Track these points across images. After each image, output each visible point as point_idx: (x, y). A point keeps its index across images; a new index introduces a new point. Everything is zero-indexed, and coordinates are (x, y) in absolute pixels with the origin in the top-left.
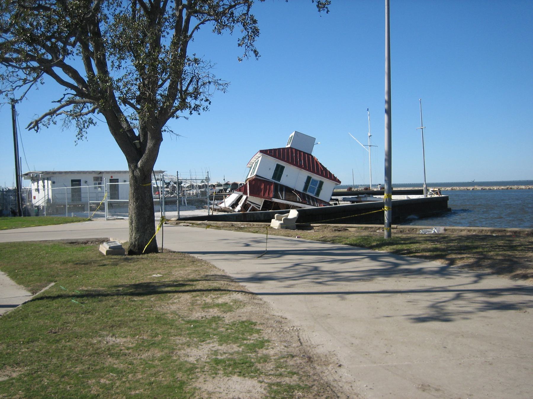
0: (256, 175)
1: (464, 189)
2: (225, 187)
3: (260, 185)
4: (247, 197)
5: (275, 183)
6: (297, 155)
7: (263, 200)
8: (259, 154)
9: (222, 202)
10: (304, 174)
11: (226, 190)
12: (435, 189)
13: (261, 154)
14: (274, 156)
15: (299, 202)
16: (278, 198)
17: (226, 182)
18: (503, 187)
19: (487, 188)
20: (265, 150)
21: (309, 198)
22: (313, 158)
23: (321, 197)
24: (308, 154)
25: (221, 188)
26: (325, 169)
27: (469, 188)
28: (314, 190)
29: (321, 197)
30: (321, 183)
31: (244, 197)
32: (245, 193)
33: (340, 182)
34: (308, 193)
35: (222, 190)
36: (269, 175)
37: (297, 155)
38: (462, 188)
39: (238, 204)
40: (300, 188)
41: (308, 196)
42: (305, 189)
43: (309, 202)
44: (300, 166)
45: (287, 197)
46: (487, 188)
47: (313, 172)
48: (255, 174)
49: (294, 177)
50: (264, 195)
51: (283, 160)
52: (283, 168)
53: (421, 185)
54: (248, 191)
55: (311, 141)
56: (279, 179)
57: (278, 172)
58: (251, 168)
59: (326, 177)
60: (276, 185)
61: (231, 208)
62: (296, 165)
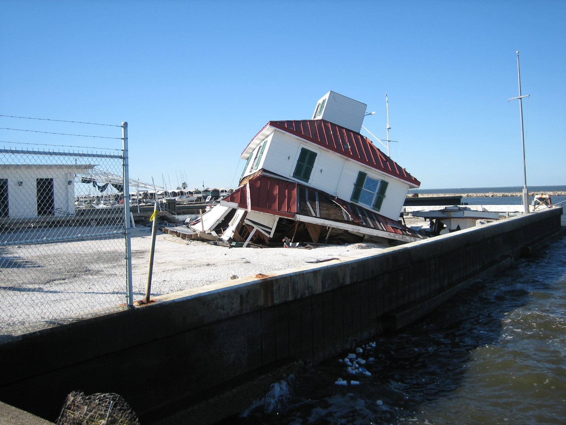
0: (264, 170)
1: (482, 196)
3: (272, 190)
4: (246, 213)
5: (299, 185)
6: (336, 135)
7: (277, 218)
8: (269, 130)
9: (198, 222)
10: (353, 168)
11: (205, 198)
12: (544, 196)
13: (273, 128)
14: (297, 133)
15: (348, 222)
16: (308, 214)
17: (205, 188)
19: (509, 194)
20: (280, 122)
21: (363, 214)
23: (386, 210)
24: (354, 132)
27: (487, 194)
28: (372, 198)
29: (386, 210)
30: (384, 185)
31: (240, 213)
32: (243, 204)
33: (418, 183)
34: (360, 204)
35: (200, 198)
36: (287, 169)
37: (336, 135)
38: (480, 195)
39: (228, 226)
40: (345, 192)
41: (361, 209)
42: (356, 195)
43: (366, 221)
44: (346, 153)
45: (324, 212)
46: (509, 194)
47: (370, 164)
48: (260, 167)
49: (334, 174)
50: (280, 208)
51: (314, 140)
52: (313, 155)
53: (520, 189)
54: (249, 201)
55: (360, 109)
57: (305, 165)
58: (248, 159)
59: (395, 174)
60: (302, 188)
61: (214, 234)
62: (338, 150)
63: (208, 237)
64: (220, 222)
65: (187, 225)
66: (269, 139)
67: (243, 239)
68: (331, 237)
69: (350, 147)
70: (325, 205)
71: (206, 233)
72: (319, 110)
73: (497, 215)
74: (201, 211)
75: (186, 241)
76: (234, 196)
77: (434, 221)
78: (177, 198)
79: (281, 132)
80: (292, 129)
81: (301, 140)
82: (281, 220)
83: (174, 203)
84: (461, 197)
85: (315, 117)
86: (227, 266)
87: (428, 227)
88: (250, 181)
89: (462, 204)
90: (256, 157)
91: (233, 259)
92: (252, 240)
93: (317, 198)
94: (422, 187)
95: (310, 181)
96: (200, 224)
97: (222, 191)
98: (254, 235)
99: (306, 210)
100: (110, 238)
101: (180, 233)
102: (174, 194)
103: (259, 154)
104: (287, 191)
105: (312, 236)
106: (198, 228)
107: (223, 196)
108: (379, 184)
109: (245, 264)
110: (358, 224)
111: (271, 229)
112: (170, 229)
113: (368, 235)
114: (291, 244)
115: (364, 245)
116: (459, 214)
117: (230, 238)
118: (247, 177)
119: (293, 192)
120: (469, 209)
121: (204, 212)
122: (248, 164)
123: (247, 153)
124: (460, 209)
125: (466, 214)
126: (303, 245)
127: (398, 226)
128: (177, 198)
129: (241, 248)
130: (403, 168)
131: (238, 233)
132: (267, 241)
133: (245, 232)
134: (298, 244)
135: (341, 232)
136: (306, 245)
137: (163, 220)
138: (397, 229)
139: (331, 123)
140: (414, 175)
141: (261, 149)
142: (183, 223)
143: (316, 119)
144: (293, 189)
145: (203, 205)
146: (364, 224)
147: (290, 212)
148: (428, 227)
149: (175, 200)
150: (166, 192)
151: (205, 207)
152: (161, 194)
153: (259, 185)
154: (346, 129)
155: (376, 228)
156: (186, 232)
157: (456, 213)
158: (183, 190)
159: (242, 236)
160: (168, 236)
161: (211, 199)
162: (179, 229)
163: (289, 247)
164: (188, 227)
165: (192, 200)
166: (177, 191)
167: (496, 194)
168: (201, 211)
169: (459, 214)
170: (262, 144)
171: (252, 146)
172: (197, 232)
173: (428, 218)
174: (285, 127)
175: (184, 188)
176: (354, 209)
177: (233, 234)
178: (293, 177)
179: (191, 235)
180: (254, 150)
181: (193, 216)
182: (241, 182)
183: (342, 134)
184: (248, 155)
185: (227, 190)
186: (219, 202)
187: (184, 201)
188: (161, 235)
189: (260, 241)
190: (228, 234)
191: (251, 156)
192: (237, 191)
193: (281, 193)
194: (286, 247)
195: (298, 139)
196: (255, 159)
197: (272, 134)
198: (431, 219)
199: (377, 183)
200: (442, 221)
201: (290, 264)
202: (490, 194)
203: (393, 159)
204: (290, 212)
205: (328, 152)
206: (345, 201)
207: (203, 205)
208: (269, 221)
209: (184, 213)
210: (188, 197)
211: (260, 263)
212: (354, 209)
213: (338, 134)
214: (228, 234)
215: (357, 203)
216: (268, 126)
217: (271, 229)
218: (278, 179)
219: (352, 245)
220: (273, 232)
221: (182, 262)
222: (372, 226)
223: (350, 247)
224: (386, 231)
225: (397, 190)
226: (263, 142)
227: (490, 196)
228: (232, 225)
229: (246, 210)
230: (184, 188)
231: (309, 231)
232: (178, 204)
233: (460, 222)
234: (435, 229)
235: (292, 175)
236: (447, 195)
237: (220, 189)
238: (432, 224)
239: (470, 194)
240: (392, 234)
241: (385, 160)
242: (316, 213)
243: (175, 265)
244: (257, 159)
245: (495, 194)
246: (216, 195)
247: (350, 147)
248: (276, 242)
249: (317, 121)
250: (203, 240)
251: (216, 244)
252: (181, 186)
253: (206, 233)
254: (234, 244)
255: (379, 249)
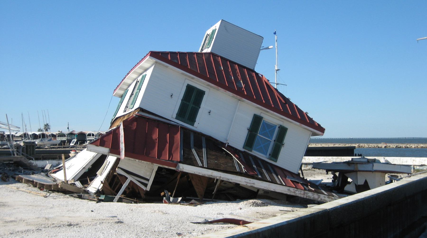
0: (141, 109)
1: (374, 147)
2: (69, 138)
3: (151, 133)
4: (118, 160)
5: (183, 128)
7: (156, 167)
8: (148, 63)
9: (59, 169)
10: (247, 110)
11: (70, 141)
13: (154, 60)
14: (183, 67)
15: (240, 174)
16: (193, 163)
17: (71, 131)
18: (422, 145)
19: (403, 146)
21: (258, 165)
22: (259, 78)
23: (283, 161)
24: (248, 69)
25: (64, 139)
26: (287, 101)
27: (380, 145)
29: (283, 161)
30: (283, 131)
31: (111, 160)
32: (115, 150)
33: (322, 130)
34: (255, 153)
35: (64, 142)
36: (169, 110)
38: (372, 145)
39: (95, 175)
40: (237, 139)
41: (256, 159)
42: (250, 141)
43: (262, 174)
44: (239, 92)
46: (403, 146)
47: (267, 105)
48: (137, 106)
49: (224, 117)
50: (159, 155)
51: (202, 76)
52: (201, 94)
54: (122, 146)
55: (256, 43)
56: (192, 119)
57: (191, 105)
58: (122, 97)
60: (186, 132)
61: (78, 184)
62: (230, 88)
63: (71, 189)
64: (86, 170)
65: (47, 173)
66: (149, 73)
67: (114, 192)
68: (219, 191)
69: (243, 86)
70: (214, 153)
71: (69, 183)
72: (207, 42)
73: (407, 170)
74: (63, 157)
75: (44, 193)
76: (105, 139)
77: (337, 174)
78: (37, 142)
79: (163, 65)
80: (176, 61)
81: (186, 75)
82: (160, 169)
83: (33, 146)
84: (355, 147)
85: (202, 50)
86: (94, 227)
87: (330, 181)
88: (124, 122)
89: (356, 156)
90: (132, 94)
91: (102, 217)
92: (124, 193)
93: (204, 144)
94: (326, 136)
95: (196, 124)
96: (62, 171)
97: (89, 135)
98: (128, 188)
99: (191, 159)
100: (89, 162)
101: (36, 183)
102: (35, 136)
103: (136, 91)
104: (168, 135)
105: (197, 190)
106: (59, 176)
107: (90, 140)
108: (277, 130)
109: (116, 225)
110: (252, 177)
111: (148, 180)
112: (25, 177)
113: (263, 190)
114: (171, 199)
115: (259, 201)
116: (368, 167)
117: (98, 190)
118: (119, 117)
119: (176, 136)
120: (379, 162)
121: (67, 157)
122: (121, 102)
123: (121, 89)
124: (369, 161)
125: (376, 167)
126: (186, 200)
127: (297, 179)
128: (37, 142)
129: (111, 203)
130: (305, 112)
131: (107, 184)
132: (142, 195)
133: (116, 184)
134: (180, 199)
135: (231, 185)
136: (191, 200)
137: (18, 166)
138: (298, 183)
139: (222, 58)
140: (317, 119)
141: (138, 85)
142: (42, 170)
143: (204, 51)
144: (176, 133)
145: (67, 149)
146: (260, 176)
147: (171, 160)
148: (330, 181)
149: (34, 143)
150: (25, 134)
151: (69, 152)
152: (21, 136)
153: (135, 128)
154: (239, 66)
155: (273, 181)
156: (44, 181)
157: (364, 165)
158: (44, 132)
159: (112, 189)
160: (22, 186)
161: (77, 143)
162: (35, 177)
163: (170, 202)
164: (47, 175)
165: (55, 143)
166: (38, 133)
167: (390, 145)
168: (63, 157)
169: (368, 167)
170: (140, 79)
171: (127, 80)
172: (58, 182)
173: (330, 170)
174: (168, 59)
175: (47, 130)
176: (246, 158)
177: (102, 185)
178: (177, 118)
179: (50, 186)
180: (129, 86)
181: (55, 162)
182: (112, 124)
183: (234, 70)
184: (122, 92)
185: (95, 133)
186: (85, 147)
187: (46, 144)
188: (14, 185)
189: (134, 195)
190: (96, 184)
191: (126, 91)
192: (108, 134)
193: (162, 137)
194: (165, 203)
195: (183, 74)
196: (131, 96)
197: (153, 67)
198: (334, 171)
199: (275, 128)
200: (347, 175)
201: (173, 225)
202: (383, 145)
203: (294, 101)
204: (171, 160)
205: (218, 90)
206: (236, 149)
207: (67, 149)
208: (145, 170)
209: (44, 159)
210: (51, 140)
211: (136, 224)
212: (246, 158)
213: (230, 70)
214: (96, 184)
215: (251, 151)
216: (148, 57)
217: (148, 180)
218: (158, 121)
219: (245, 202)
220: (150, 184)
221: (36, 220)
222: (269, 179)
223: (242, 204)
224: (286, 185)
225: (296, 137)
226: (141, 77)
227: (383, 147)
228: (101, 174)
229: (119, 156)
230: (47, 130)
231: (193, 183)
232: (38, 148)
233: (370, 178)
234: (338, 184)
235: (175, 116)
236: (337, 145)
237: (87, 132)
238: (335, 177)
239: (361, 145)
240: (292, 189)
241: (283, 101)
242: (202, 163)
243: (28, 224)
244: (133, 96)
245: (388, 145)
246: (82, 138)
247: (243, 86)
248: (153, 197)
249: (205, 54)
250: (65, 192)
251: (80, 197)
252: (42, 127)
253: (69, 183)
254: (102, 197)
255: (279, 207)
